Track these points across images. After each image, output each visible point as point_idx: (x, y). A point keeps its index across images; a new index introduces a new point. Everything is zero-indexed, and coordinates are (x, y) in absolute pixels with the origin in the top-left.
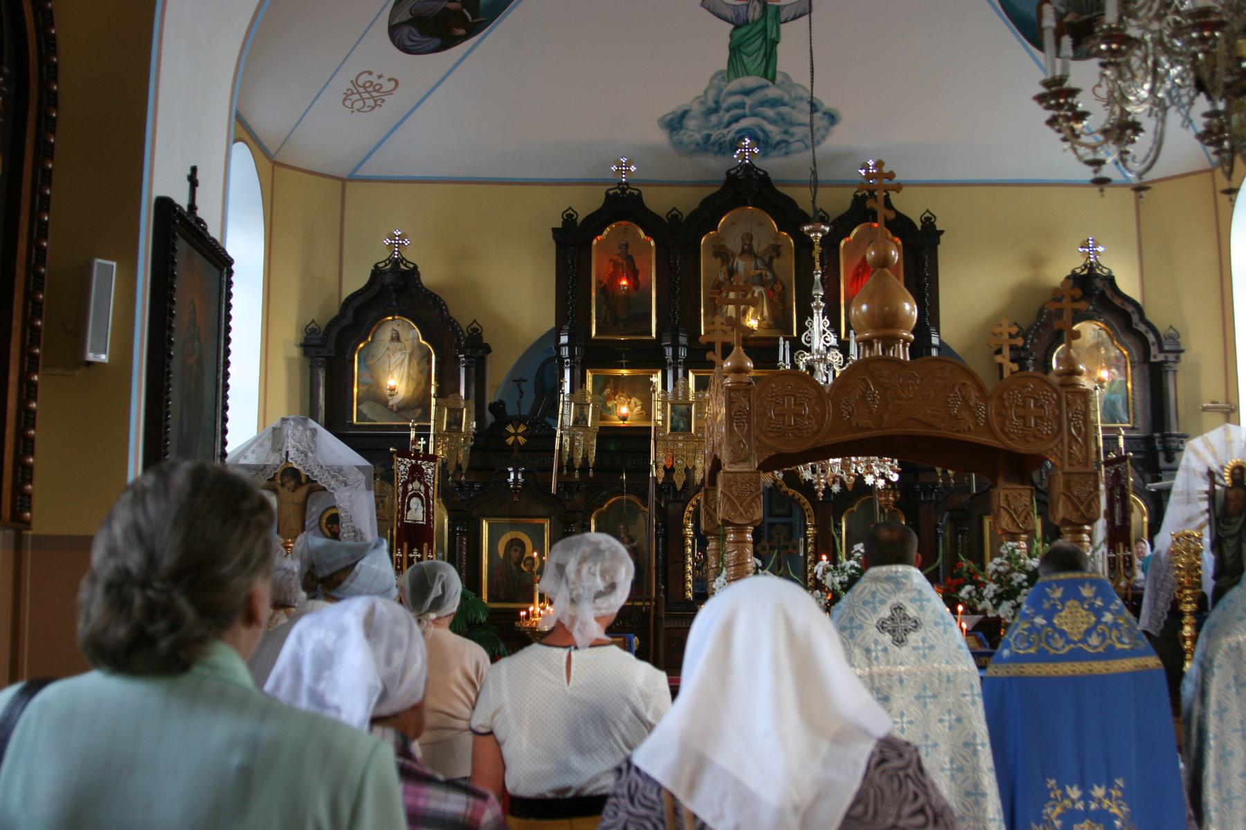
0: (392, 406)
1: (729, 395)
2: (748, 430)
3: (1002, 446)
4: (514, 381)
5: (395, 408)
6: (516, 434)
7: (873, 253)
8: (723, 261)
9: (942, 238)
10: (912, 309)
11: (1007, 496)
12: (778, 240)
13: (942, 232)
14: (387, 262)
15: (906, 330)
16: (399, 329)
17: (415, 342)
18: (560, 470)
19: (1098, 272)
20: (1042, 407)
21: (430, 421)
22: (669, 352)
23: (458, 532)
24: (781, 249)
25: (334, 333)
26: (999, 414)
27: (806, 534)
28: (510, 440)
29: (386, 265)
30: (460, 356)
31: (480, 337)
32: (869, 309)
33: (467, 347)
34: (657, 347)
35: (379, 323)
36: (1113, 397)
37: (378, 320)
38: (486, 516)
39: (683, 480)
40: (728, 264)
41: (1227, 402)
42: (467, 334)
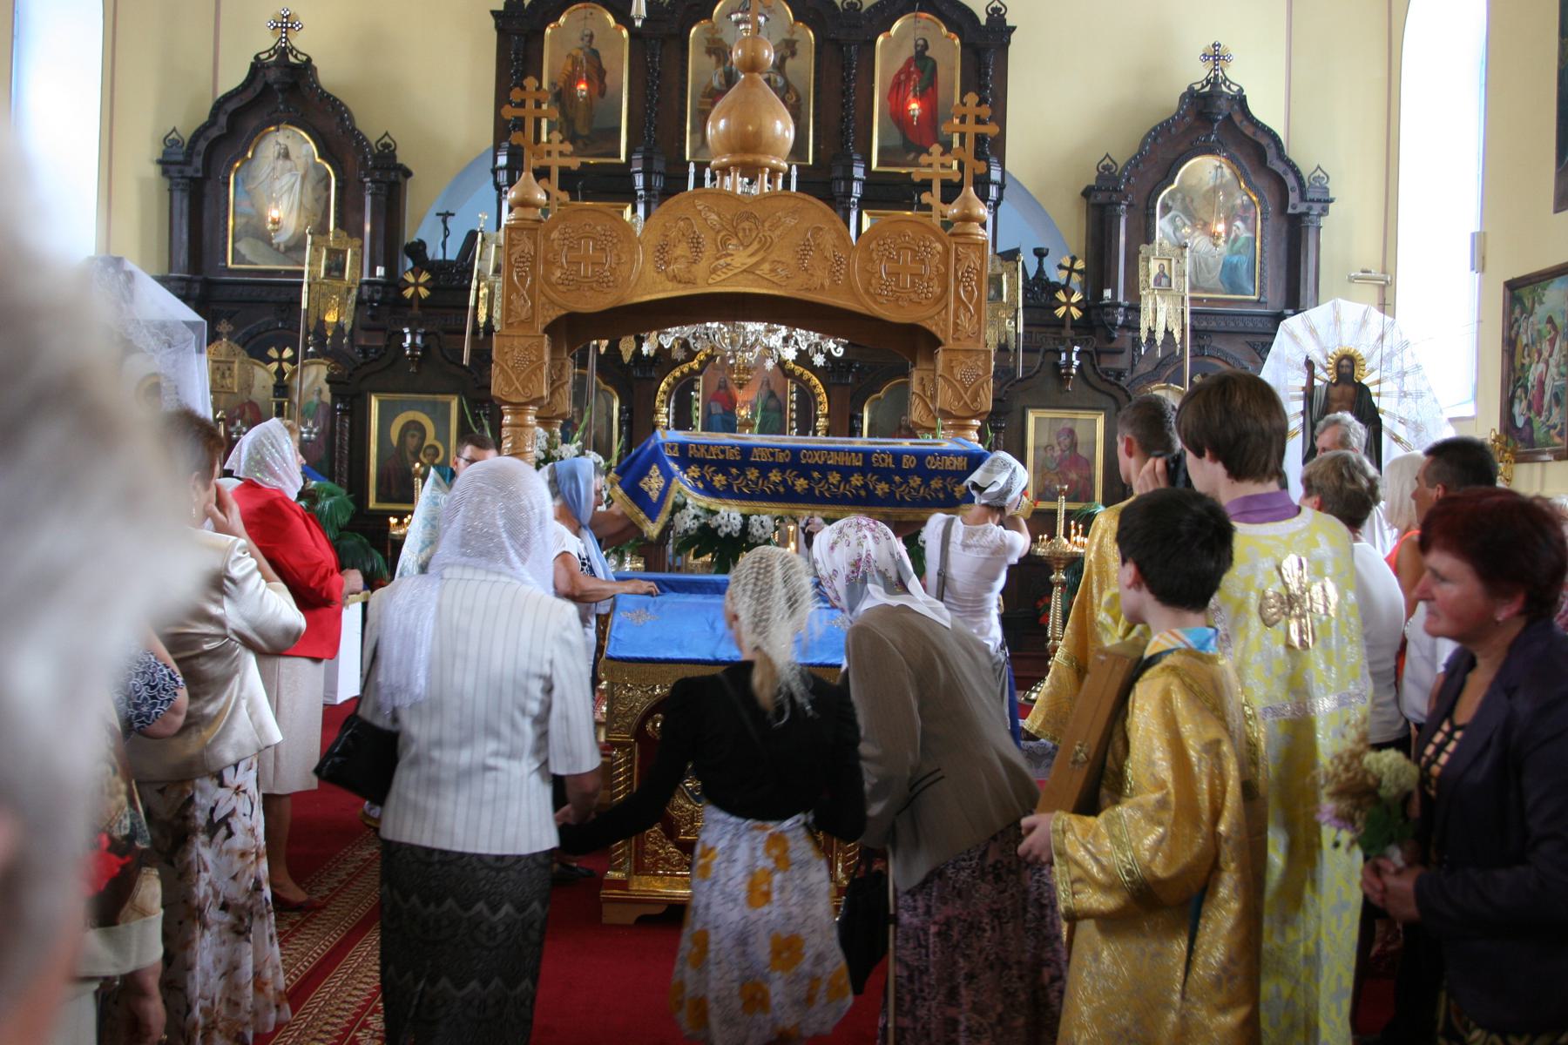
0: (279, 244)
1: (510, 235)
2: (530, 286)
3: (862, 310)
4: (438, 214)
5: (282, 248)
6: (416, 285)
7: (740, 52)
8: (718, 61)
9: (1014, 37)
10: (787, 128)
11: (922, 379)
12: (794, 32)
13: (1014, 28)
14: (272, 52)
15: (776, 155)
16: (289, 143)
17: (310, 161)
18: (475, 332)
19: (1224, 89)
20: (922, 261)
21: (303, 265)
22: (639, 181)
23: (339, 410)
24: (797, 46)
25: (202, 145)
26: (863, 270)
27: (815, 426)
28: (1061, 312)
29: (270, 56)
30: (365, 180)
31: (393, 155)
32: (727, 126)
33: (375, 168)
34: (625, 174)
35: (262, 133)
36: (1235, 259)
37: (259, 132)
38: (376, 391)
39: (631, 350)
40: (724, 64)
41: (1384, 272)
42: (376, 151)
